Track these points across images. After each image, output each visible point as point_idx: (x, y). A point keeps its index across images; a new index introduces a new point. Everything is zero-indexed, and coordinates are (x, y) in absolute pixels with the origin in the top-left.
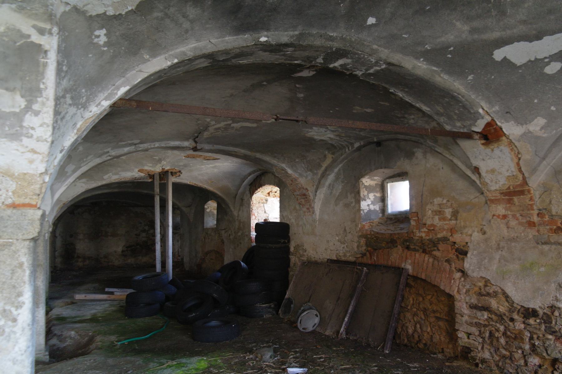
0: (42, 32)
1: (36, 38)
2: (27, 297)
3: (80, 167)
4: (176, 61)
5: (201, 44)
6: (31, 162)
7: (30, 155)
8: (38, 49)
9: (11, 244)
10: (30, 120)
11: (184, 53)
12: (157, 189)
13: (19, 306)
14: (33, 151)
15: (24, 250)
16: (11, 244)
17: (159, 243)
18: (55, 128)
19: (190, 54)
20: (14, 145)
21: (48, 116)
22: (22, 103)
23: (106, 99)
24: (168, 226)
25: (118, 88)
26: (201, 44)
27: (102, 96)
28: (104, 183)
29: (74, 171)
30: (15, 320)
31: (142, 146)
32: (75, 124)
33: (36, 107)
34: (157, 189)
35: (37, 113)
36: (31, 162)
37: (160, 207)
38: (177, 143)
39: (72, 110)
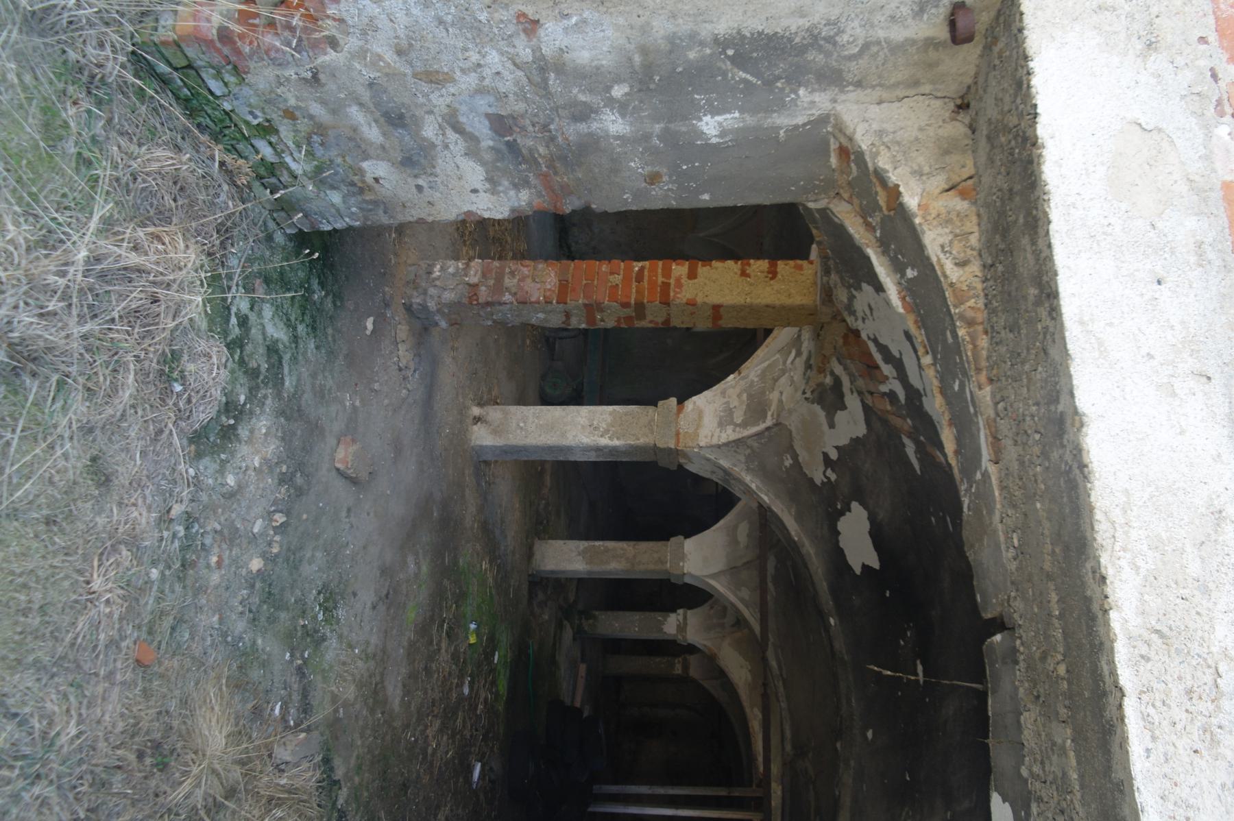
0: (772, 415)
1: (769, 414)
2: (616, 443)
3: (747, 607)
4: (796, 539)
5: (814, 559)
6: (706, 437)
7: (710, 434)
8: (764, 418)
9: (652, 433)
10: (730, 429)
11: (803, 546)
12: (737, 792)
13: (610, 438)
14: (712, 436)
15: (647, 440)
16: (652, 433)
17: (650, 792)
18: (727, 444)
19: (804, 551)
20: (716, 425)
21: (733, 437)
22: (739, 421)
23: (757, 486)
24: (677, 808)
25: (766, 495)
26: (814, 559)
27: (759, 483)
28: (748, 710)
29: (742, 600)
30: (602, 436)
31: (781, 683)
32: (735, 466)
33: (738, 429)
34: (737, 792)
35: (734, 431)
36: (706, 437)
37: (705, 797)
38: (788, 734)
39: (743, 459)
